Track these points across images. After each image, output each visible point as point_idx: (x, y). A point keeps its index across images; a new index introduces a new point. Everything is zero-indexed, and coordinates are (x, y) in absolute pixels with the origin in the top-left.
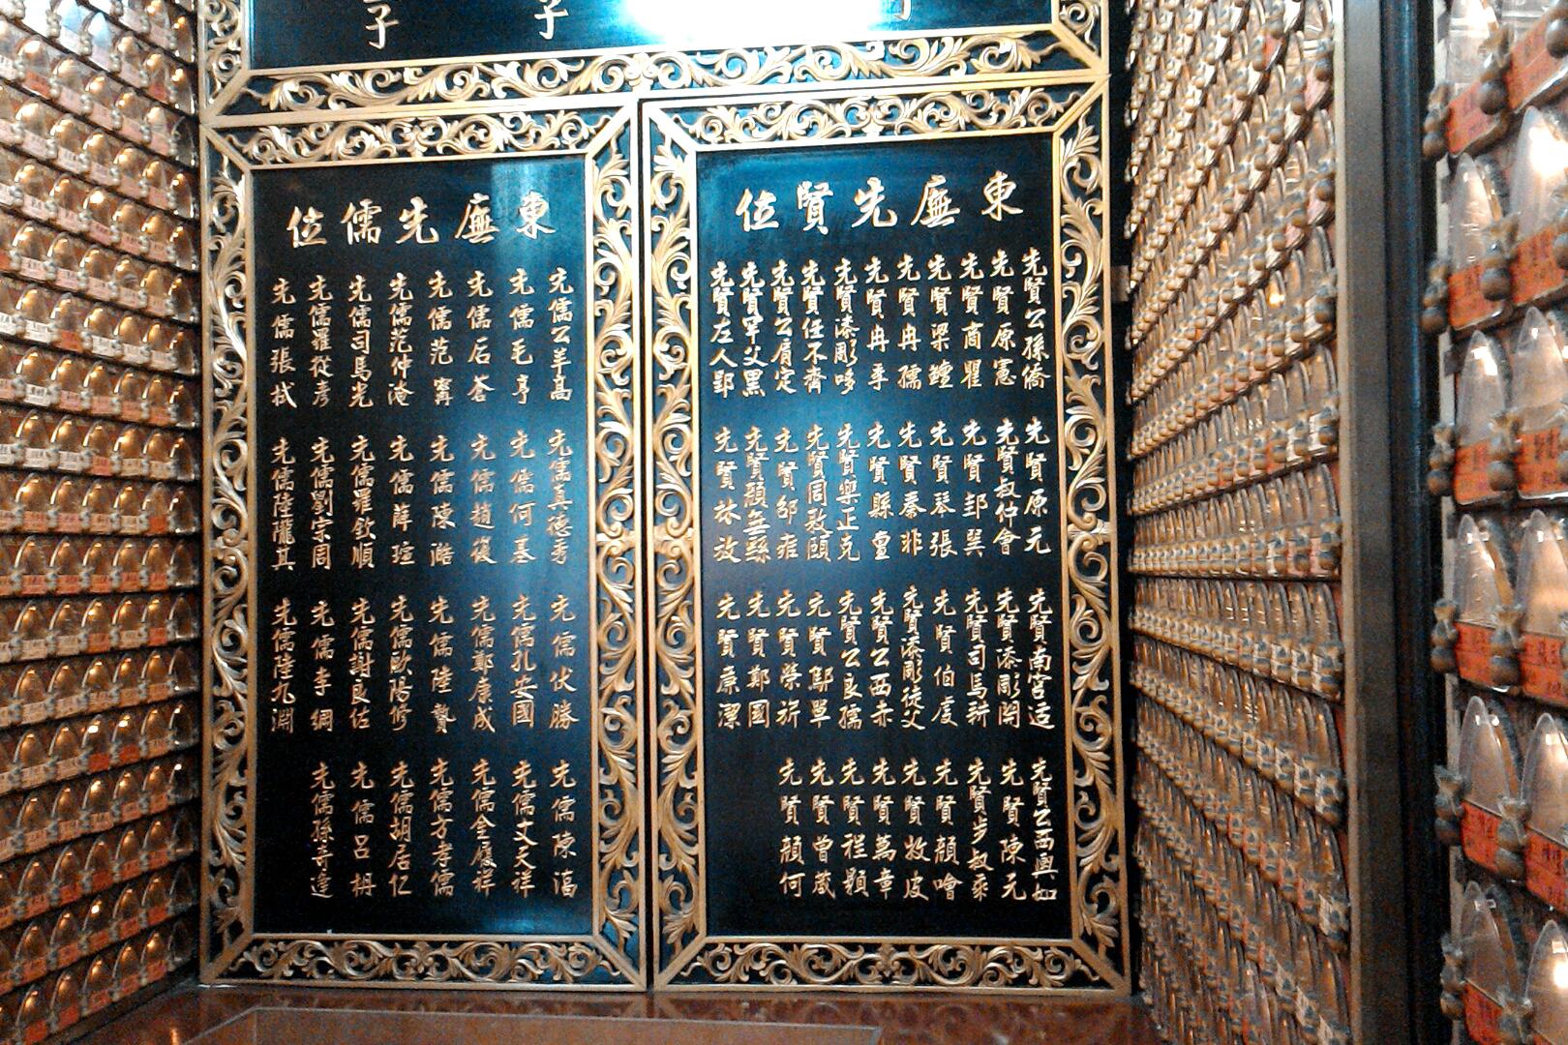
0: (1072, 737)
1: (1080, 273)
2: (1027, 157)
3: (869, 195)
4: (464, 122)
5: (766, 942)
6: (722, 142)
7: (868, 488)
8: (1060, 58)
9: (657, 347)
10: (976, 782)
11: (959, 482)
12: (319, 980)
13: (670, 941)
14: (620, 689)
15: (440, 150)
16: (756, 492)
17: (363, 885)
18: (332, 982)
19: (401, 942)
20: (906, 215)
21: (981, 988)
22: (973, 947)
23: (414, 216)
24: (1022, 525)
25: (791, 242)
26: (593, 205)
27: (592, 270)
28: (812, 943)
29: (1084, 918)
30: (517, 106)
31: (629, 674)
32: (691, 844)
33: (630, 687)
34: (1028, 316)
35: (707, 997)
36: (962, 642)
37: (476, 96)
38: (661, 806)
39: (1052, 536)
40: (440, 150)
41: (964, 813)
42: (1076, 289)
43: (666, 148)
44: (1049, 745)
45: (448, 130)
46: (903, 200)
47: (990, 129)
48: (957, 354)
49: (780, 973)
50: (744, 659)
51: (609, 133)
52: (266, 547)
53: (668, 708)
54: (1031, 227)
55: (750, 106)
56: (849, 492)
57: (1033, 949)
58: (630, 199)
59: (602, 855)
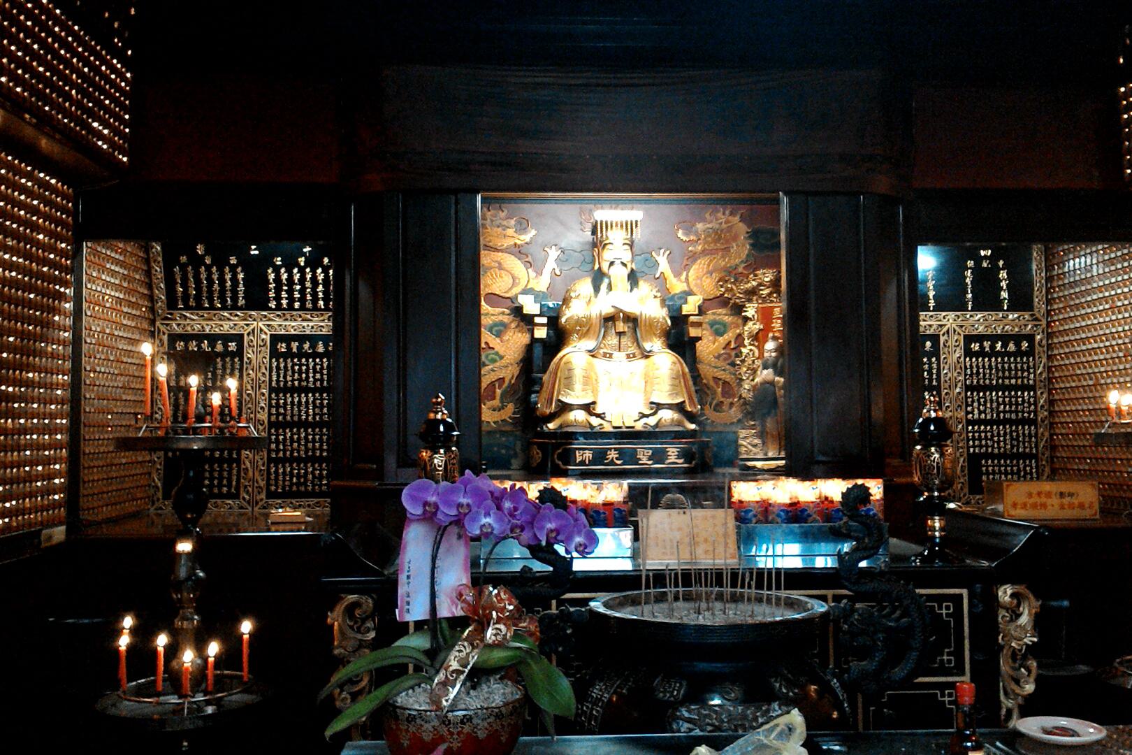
2: (1030, 338)
7: (999, 404)
8: (1037, 319)
9: (260, 375)
11: (1017, 404)
16: (976, 404)
24: (1029, 413)
25: (289, 354)
26: (246, 344)
36: (1018, 436)
39: (1035, 415)
41: (1019, 470)
44: (1035, 456)
46: (313, 346)
47: (1023, 332)
48: (1017, 378)
50: (974, 439)
54: (1030, 352)
56: (995, 405)
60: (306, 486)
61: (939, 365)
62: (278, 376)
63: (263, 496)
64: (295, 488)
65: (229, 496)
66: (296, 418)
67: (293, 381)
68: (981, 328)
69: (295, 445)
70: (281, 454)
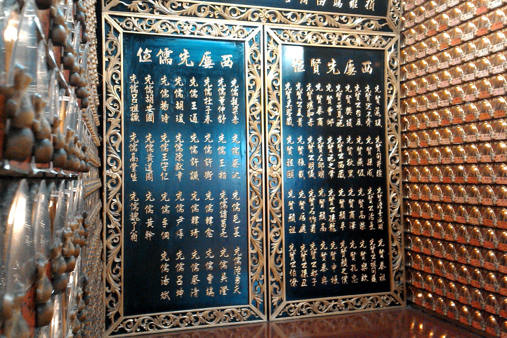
0: (391, 232)
1: (254, 88)
3: (184, 54)
4: (204, 25)
5: (147, 316)
6: (339, 44)
10: (292, 251)
12: (151, 331)
13: (274, 304)
14: (257, 221)
15: (341, 44)
17: (210, 292)
18: (156, 331)
19: (181, 313)
20: (342, 71)
21: (367, 310)
22: (218, 310)
23: (332, 65)
27: (387, 84)
28: (163, 314)
29: (394, 285)
30: (221, 22)
31: (261, 216)
32: (280, 272)
33: (261, 220)
34: (298, 103)
35: (287, 321)
37: (208, 17)
38: (271, 260)
40: (341, 44)
42: (390, 96)
43: (272, 41)
45: (199, 26)
49: (309, 311)
51: (253, 35)
52: (128, 171)
53: (273, 227)
54: (377, 78)
55: (298, 31)
57: (238, 309)
58: (260, 57)
59: (252, 277)
60: (340, 276)
61: (242, 91)
62: (295, 111)
63: (283, 293)
64: (324, 280)
65: (230, 299)
66: (321, 174)
67: (316, 117)
68: (358, 41)
69: (322, 215)
70: (303, 229)
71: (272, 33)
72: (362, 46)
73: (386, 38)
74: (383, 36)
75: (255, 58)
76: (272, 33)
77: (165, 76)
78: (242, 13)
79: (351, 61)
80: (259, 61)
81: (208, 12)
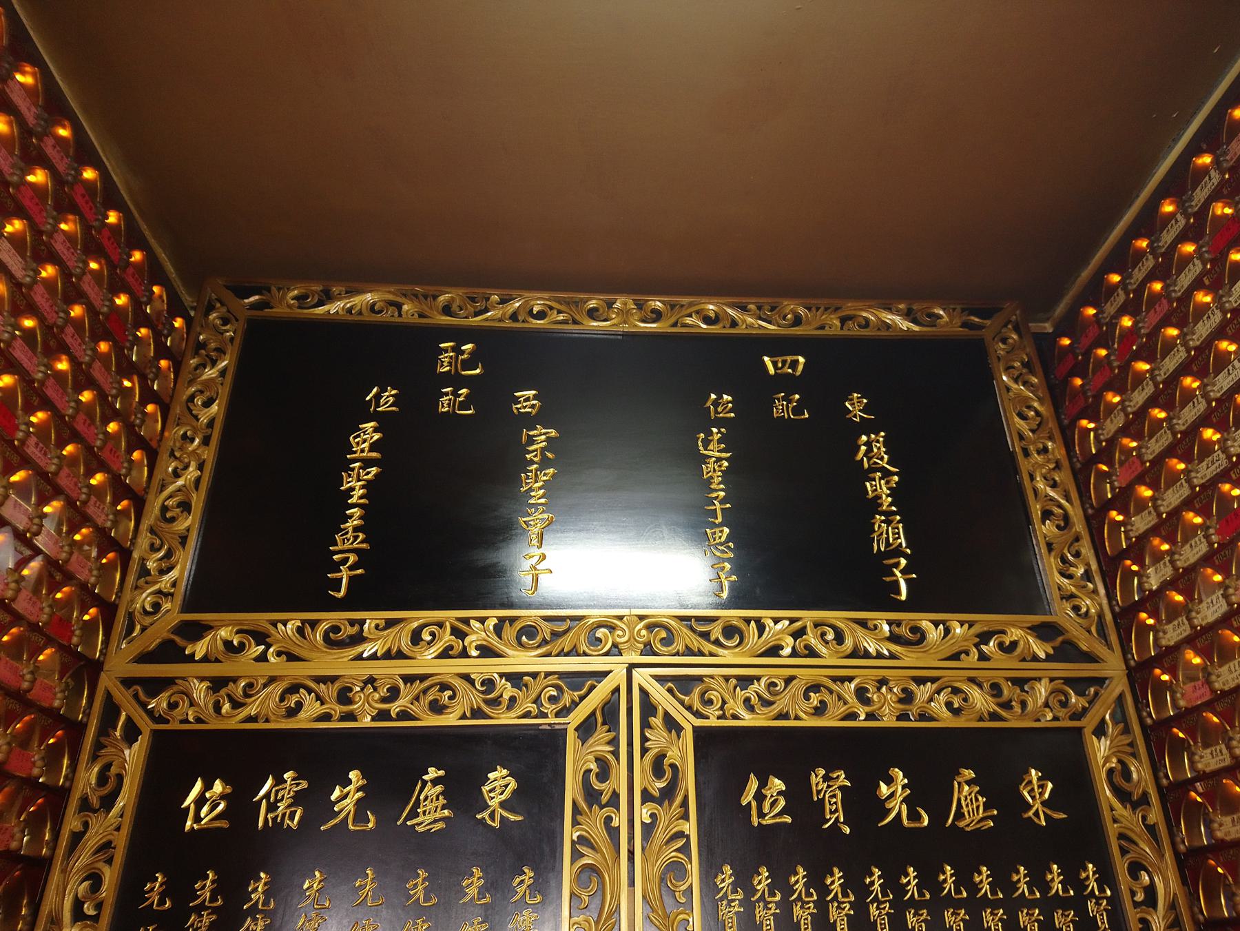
20: (938, 816)
23: (894, 790)
37: (445, 654)
43: (657, 721)
54: (1078, 836)
71: (659, 694)
72: (994, 716)
73: (1080, 685)
74: (1068, 681)
75: (597, 786)
76: (659, 694)
77: (836, 870)
78: (556, 635)
79: (969, 774)
80: (615, 795)
81: (447, 638)
